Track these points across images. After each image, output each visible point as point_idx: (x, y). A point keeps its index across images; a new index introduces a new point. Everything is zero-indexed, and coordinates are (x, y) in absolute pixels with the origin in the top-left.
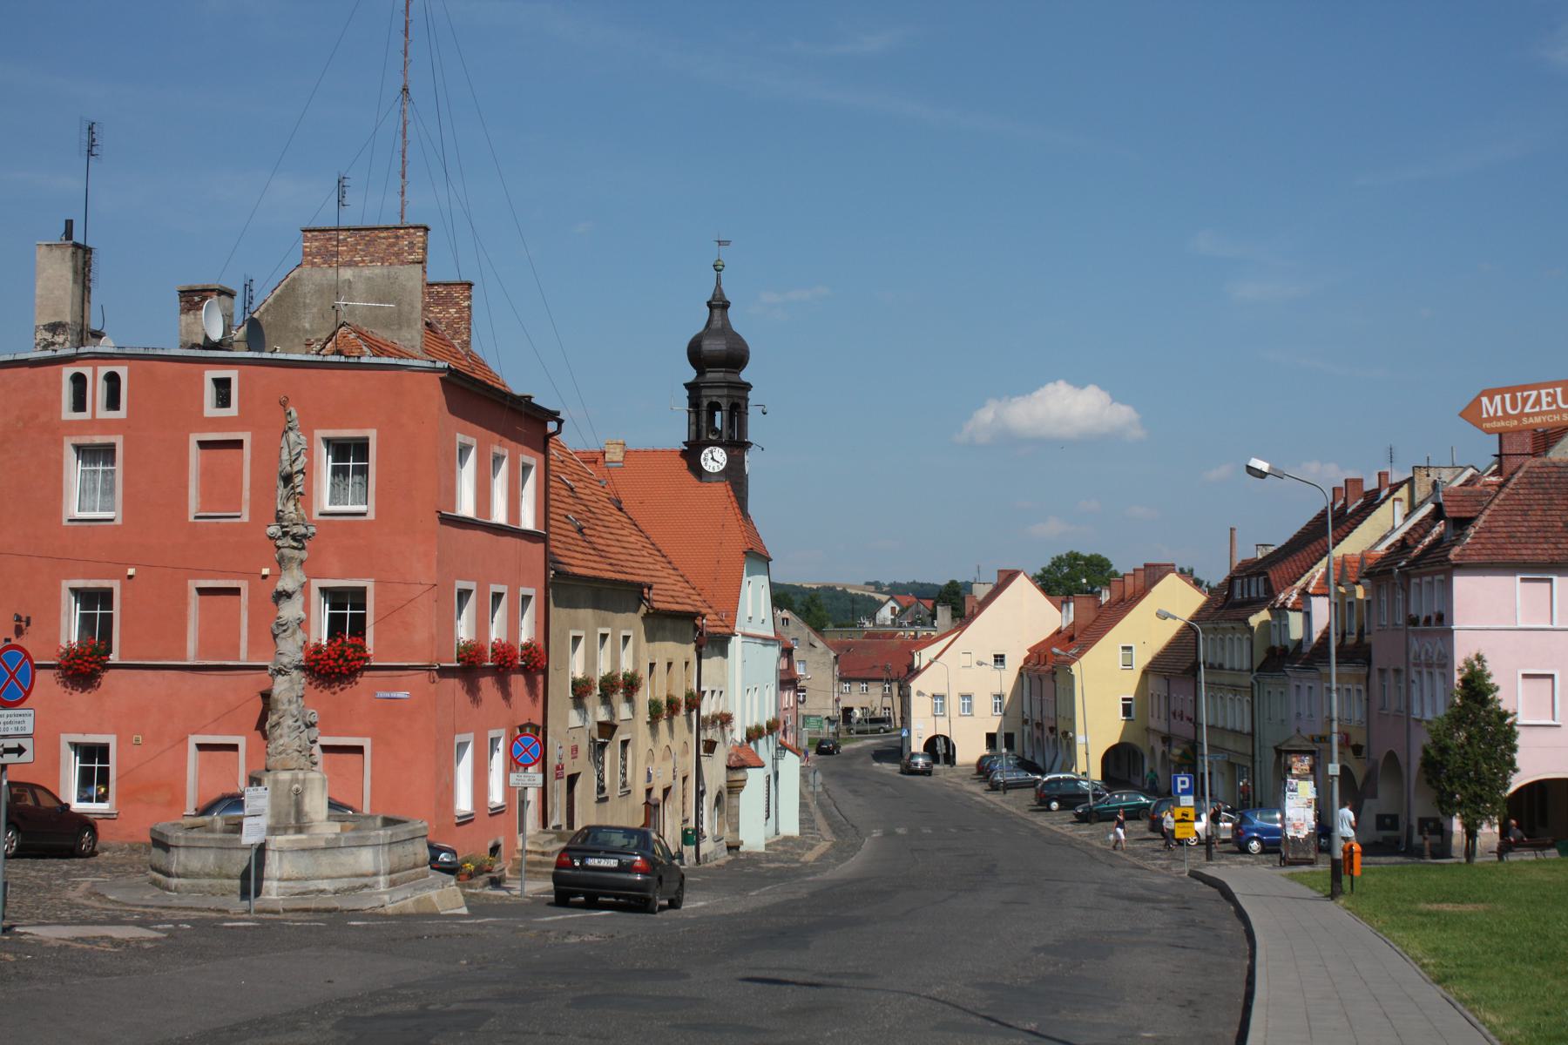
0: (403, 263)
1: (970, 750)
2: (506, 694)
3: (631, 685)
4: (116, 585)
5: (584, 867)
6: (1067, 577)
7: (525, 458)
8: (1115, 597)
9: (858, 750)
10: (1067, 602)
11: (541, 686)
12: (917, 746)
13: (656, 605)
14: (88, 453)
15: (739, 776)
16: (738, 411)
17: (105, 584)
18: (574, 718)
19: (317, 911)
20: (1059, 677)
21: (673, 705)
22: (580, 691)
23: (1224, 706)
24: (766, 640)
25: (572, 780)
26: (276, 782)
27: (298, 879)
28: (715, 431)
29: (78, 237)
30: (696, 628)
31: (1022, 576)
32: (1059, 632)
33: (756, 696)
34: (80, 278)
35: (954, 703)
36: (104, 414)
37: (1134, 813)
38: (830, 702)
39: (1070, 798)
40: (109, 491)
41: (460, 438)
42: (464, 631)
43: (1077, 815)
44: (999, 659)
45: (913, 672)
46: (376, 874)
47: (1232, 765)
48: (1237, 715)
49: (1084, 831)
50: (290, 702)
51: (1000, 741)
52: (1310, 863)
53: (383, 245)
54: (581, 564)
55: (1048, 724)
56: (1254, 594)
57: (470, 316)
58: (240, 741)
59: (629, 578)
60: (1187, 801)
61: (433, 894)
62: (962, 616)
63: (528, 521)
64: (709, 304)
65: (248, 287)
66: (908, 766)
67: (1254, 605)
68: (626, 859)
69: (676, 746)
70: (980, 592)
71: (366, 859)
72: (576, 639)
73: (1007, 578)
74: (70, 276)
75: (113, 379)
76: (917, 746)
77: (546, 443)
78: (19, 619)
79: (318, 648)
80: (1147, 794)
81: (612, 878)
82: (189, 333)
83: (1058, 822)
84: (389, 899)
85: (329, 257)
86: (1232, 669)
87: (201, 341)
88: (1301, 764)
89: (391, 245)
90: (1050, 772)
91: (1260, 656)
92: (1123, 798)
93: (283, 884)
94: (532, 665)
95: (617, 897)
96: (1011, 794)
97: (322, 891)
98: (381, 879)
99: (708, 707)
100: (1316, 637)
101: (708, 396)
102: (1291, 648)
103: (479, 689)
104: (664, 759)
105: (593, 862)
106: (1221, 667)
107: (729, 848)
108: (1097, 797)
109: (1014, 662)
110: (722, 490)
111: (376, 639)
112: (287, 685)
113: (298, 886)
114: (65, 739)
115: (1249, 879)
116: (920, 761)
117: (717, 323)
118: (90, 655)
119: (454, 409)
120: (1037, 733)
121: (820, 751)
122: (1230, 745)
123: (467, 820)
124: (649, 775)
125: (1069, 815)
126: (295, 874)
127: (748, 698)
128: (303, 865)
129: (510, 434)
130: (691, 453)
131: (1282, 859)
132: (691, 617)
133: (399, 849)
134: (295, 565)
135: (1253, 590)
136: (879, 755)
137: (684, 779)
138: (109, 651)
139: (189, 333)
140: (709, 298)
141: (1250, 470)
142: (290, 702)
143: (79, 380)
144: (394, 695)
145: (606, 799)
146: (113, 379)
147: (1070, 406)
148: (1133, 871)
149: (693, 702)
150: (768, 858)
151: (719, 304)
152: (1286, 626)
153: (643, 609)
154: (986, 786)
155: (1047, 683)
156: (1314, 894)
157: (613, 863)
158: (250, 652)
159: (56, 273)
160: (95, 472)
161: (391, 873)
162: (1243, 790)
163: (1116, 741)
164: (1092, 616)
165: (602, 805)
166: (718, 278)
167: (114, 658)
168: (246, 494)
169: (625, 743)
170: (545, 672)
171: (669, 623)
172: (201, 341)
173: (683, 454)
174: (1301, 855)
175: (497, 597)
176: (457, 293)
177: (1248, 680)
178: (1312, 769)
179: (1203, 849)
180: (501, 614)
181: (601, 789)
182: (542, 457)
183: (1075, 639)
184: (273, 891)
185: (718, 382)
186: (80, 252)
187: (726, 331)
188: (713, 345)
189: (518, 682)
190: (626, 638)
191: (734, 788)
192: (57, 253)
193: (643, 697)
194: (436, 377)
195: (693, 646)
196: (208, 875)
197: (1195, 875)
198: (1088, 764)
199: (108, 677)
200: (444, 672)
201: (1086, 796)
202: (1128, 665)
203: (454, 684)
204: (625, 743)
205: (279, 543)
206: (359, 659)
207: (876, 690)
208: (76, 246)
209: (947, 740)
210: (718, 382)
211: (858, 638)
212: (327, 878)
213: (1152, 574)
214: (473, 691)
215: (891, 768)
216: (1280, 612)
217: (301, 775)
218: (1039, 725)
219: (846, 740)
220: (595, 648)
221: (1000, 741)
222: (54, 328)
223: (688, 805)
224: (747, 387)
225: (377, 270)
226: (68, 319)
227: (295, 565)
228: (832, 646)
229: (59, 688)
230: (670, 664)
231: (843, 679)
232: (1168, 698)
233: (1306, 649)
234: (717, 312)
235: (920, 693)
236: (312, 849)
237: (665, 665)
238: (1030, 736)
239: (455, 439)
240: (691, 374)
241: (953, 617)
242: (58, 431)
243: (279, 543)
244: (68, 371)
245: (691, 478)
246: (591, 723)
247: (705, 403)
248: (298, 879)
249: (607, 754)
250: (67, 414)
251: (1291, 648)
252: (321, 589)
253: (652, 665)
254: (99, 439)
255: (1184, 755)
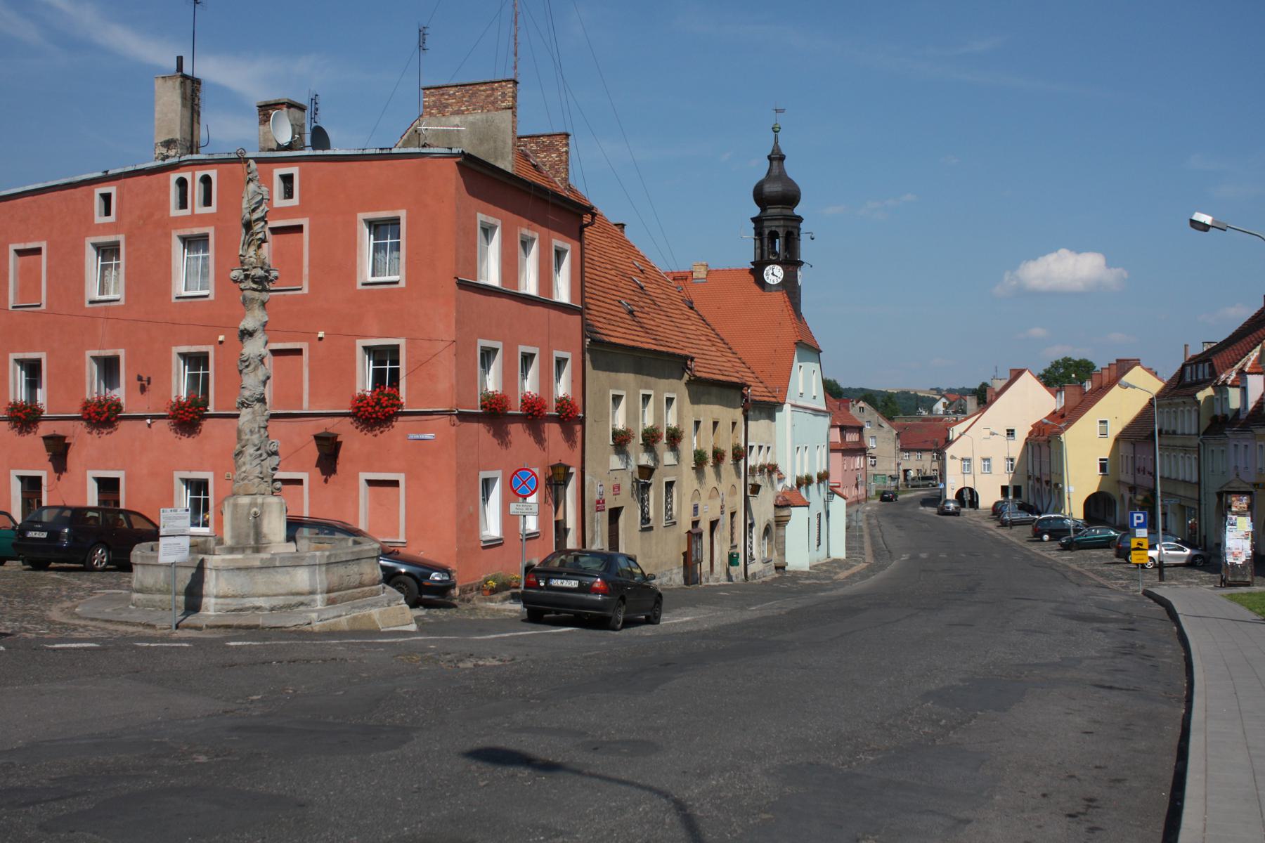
0: (497, 109)
1: (989, 496)
2: (540, 440)
3: (674, 438)
4: (210, 349)
5: (549, 587)
6: (1062, 375)
7: (557, 242)
8: (1096, 385)
9: (911, 498)
10: (1060, 391)
11: (579, 434)
12: (951, 495)
13: (698, 374)
14: (188, 242)
15: (785, 512)
16: (792, 239)
17: (202, 348)
18: (615, 462)
19: (239, 627)
20: (1053, 444)
21: (718, 456)
22: (621, 441)
23: (1177, 463)
24: (816, 412)
25: (615, 514)
26: (235, 506)
27: (234, 596)
28: (775, 253)
29: (187, 70)
30: (743, 396)
31: (1027, 374)
32: (1054, 412)
33: (806, 456)
34: (189, 103)
35: (978, 465)
36: (201, 210)
37: (1105, 544)
38: (893, 465)
39: (1058, 532)
40: (205, 275)
41: (481, 217)
42: (492, 382)
43: (1062, 545)
44: (1011, 433)
45: (948, 442)
46: (312, 593)
47: (1182, 508)
48: (1186, 469)
49: (1067, 556)
50: (252, 432)
51: (1011, 491)
52: (1247, 584)
53: (482, 95)
54: (620, 334)
55: (1045, 478)
56: (1200, 377)
57: (567, 161)
58: (305, 476)
59: (671, 350)
60: (1142, 533)
61: (375, 613)
62: (985, 402)
63: (563, 294)
64: (769, 157)
65: (314, 100)
66: (942, 509)
67: (1202, 385)
68: (587, 581)
69: (724, 487)
70: (998, 385)
71: (302, 579)
72: (617, 399)
73: (1016, 374)
74: (179, 101)
75: (206, 180)
76: (951, 495)
77: (582, 232)
78: (140, 378)
79: (362, 398)
80: (1116, 529)
81: (589, 597)
82: (266, 140)
83: (1048, 550)
84: (318, 615)
85: (442, 108)
86: (1183, 434)
87: (274, 146)
88: (1240, 503)
89: (488, 96)
90: (1046, 513)
91: (1205, 423)
92: (1097, 532)
93: (220, 601)
94: (570, 417)
95: (557, 613)
96: (1016, 529)
97: (258, 608)
98: (318, 597)
99: (754, 460)
100: (1251, 406)
101: (769, 226)
102: (1230, 416)
103: (507, 433)
104: (710, 497)
105: (556, 583)
106: (1174, 433)
107: (776, 568)
108: (1076, 531)
109: (1022, 434)
110: (780, 297)
111: (408, 388)
112: (249, 417)
113: (234, 603)
114: (178, 475)
115: (1193, 598)
116: (952, 505)
117: (775, 171)
118: (190, 406)
119: (472, 191)
120: (1037, 485)
121: (883, 499)
122: (1181, 492)
123: (494, 544)
124: (696, 508)
125: (1056, 545)
126: (231, 592)
127: (798, 456)
128: (239, 583)
129: (537, 219)
130: (757, 270)
131: (1223, 581)
132: (739, 387)
133: (341, 570)
134: (256, 306)
135: (1200, 374)
136: (926, 502)
137: (733, 514)
138: (207, 404)
139: (266, 140)
140: (769, 153)
141: (1195, 224)
142: (252, 432)
143: (182, 183)
144: (422, 436)
145: (651, 529)
146: (206, 180)
147: (1071, 267)
148: (1095, 590)
149: (739, 454)
150: (807, 575)
151: (777, 158)
152: (1227, 399)
153: (686, 377)
154: (998, 523)
155: (1045, 450)
156: (1251, 616)
157: (574, 584)
158: (310, 402)
159: (169, 99)
160: (197, 258)
161: (329, 592)
162: (1192, 527)
163: (1095, 490)
164: (1078, 399)
165: (646, 534)
166: (776, 137)
167: (211, 409)
168: (306, 270)
169: (670, 485)
170: (582, 421)
171: (714, 390)
172: (274, 146)
173: (752, 271)
174: (1239, 578)
175: (527, 359)
176: (558, 142)
177: (1195, 441)
178: (1250, 507)
179: (1157, 571)
180: (533, 371)
181: (645, 519)
182: (577, 244)
183: (1065, 417)
184: (211, 607)
185: (777, 219)
186: (188, 82)
187: (783, 177)
188: (773, 188)
189: (553, 431)
190: (669, 401)
191: (781, 522)
192: (170, 83)
193: (690, 444)
194: (452, 162)
195: (740, 410)
196: (159, 591)
197: (1148, 594)
198: (1074, 509)
199: (207, 425)
200: (464, 417)
201: (1068, 530)
202: (1104, 434)
203: (480, 431)
204: (670, 485)
205: (242, 286)
206: (393, 405)
207: (927, 457)
208: (185, 77)
209: (971, 491)
210: (777, 219)
211: (917, 422)
212: (263, 596)
213: (1123, 366)
214: (501, 435)
215: (931, 511)
216: (1222, 388)
217: (260, 500)
218: (1039, 480)
219: (904, 492)
220: (627, 406)
221: (1011, 491)
222: (168, 144)
223: (736, 535)
224: (799, 219)
225: (477, 117)
226: (178, 136)
227: (256, 306)
228: (895, 427)
229: (172, 434)
230: (715, 424)
231: (902, 450)
232: (1134, 458)
233: (1243, 416)
234: (775, 163)
235: (953, 457)
236: (247, 569)
237: (709, 425)
238: (1033, 487)
239: (476, 218)
240: (756, 211)
241: (979, 404)
242: (167, 224)
243: (242, 286)
244: (174, 176)
245: (756, 288)
246: (633, 466)
247: (767, 232)
248: (234, 596)
249: (652, 492)
250: (175, 212)
251: (1230, 416)
252: (365, 348)
253: (697, 423)
254: (197, 231)
255: (1146, 499)
